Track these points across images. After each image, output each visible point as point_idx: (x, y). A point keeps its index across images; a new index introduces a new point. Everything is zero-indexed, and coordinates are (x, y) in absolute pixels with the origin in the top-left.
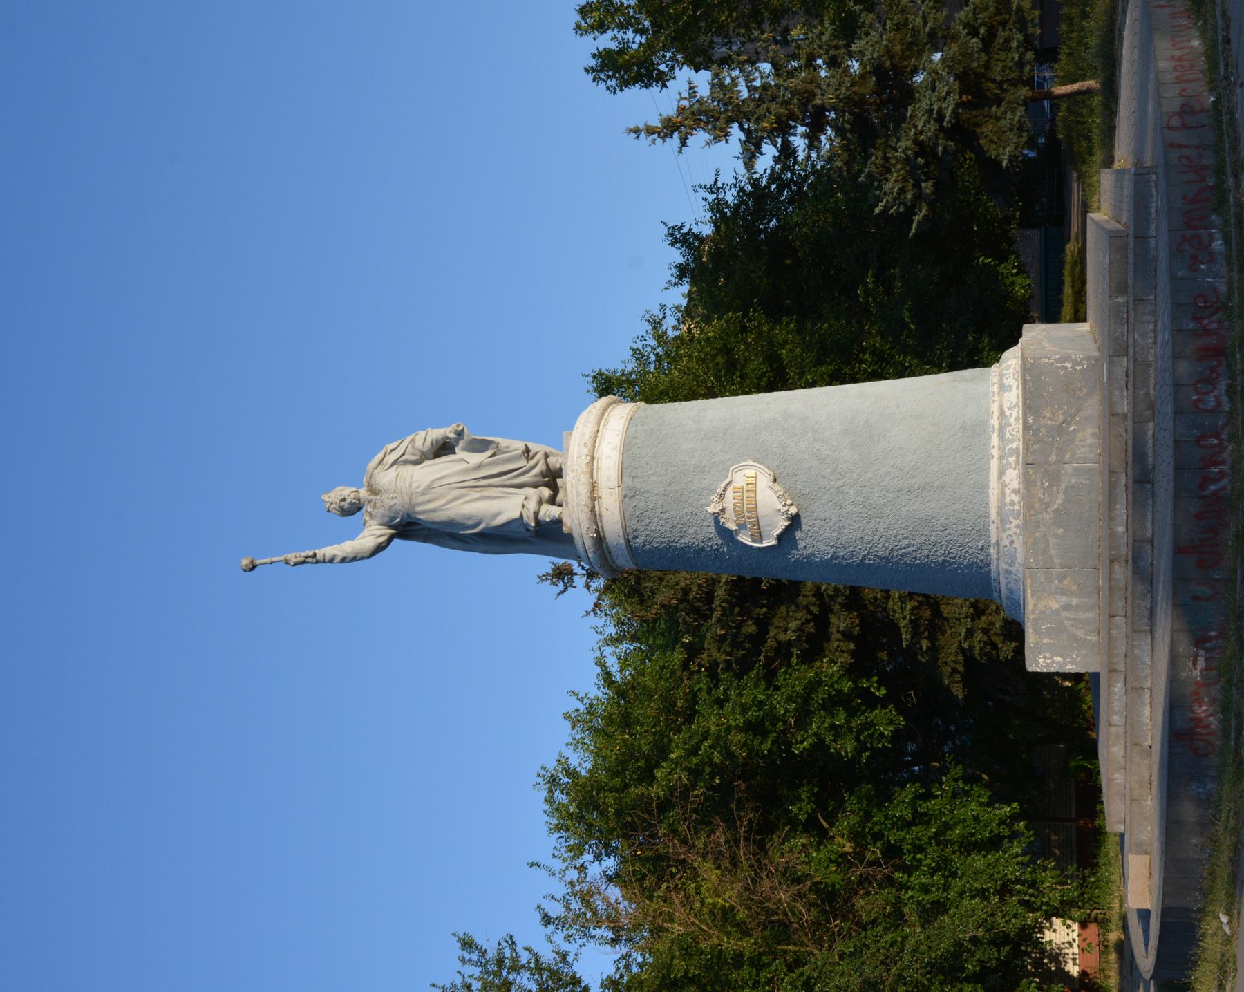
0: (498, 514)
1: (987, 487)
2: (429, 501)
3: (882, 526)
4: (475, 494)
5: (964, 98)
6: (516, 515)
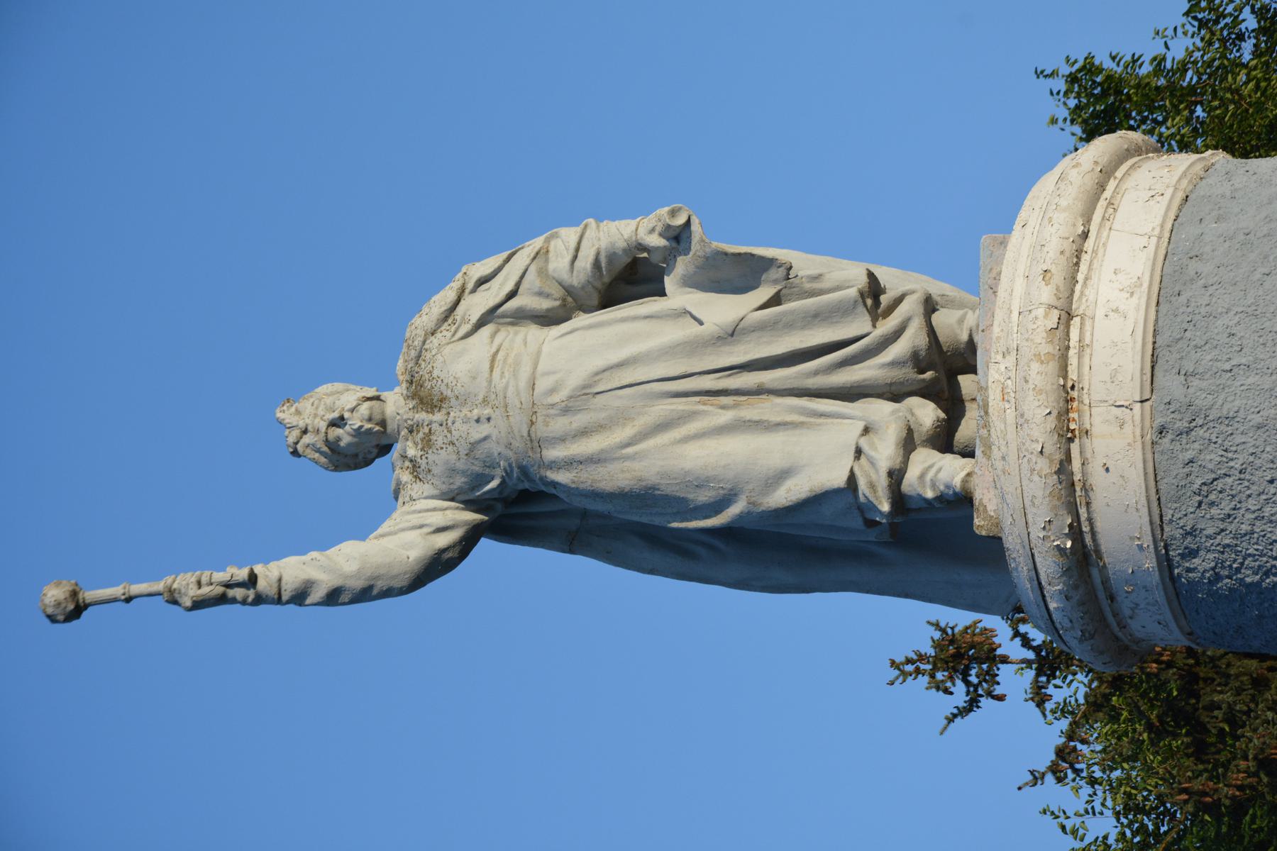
0: (783, 475)
2: (584, 432)
6: (837, 479)
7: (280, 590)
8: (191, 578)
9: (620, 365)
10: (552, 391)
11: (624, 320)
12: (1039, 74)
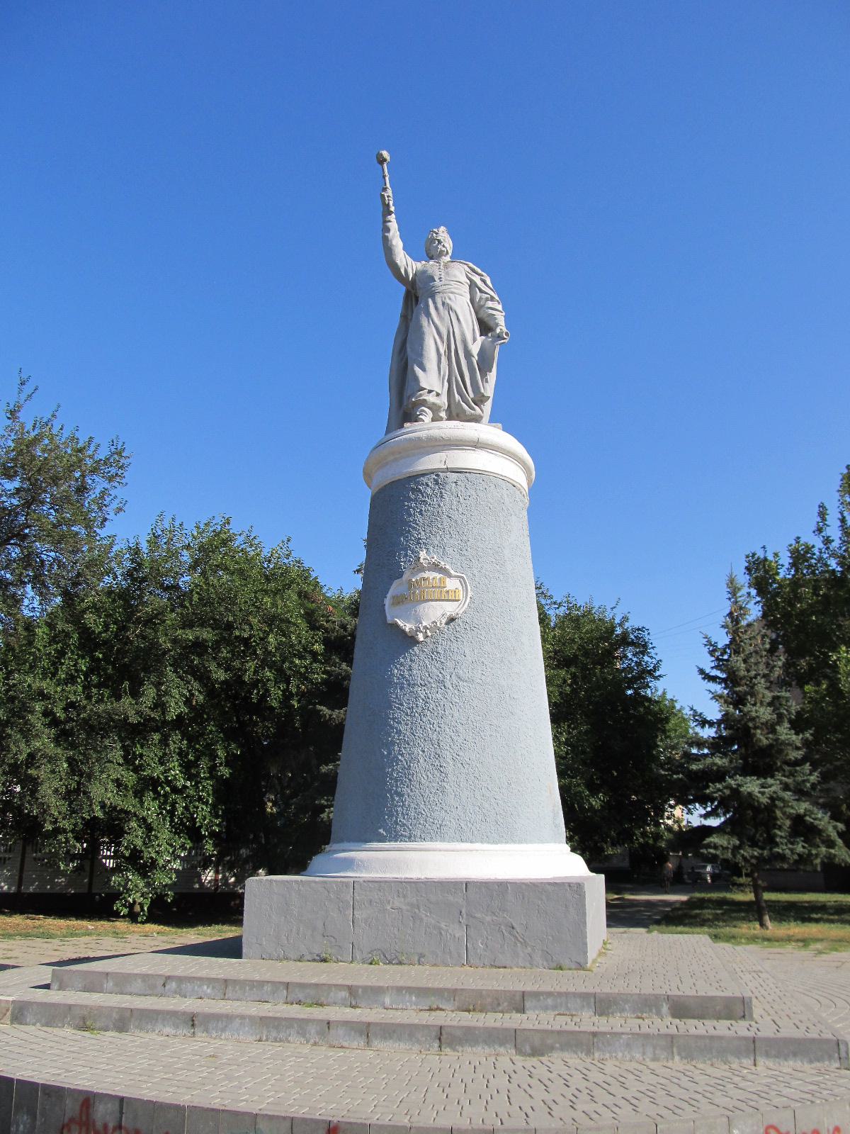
0: (424, 369)
1: (443, 840)
2: (436, 308)
3: (402, 728)
4: (442, 349)
5: (654, 1011)
6: (423, 384)
7: (428, 600)
8: (391, 194)
9: (458, 319)
10: (450, 299)
11: (473, 322)
12: (575, 1109)
